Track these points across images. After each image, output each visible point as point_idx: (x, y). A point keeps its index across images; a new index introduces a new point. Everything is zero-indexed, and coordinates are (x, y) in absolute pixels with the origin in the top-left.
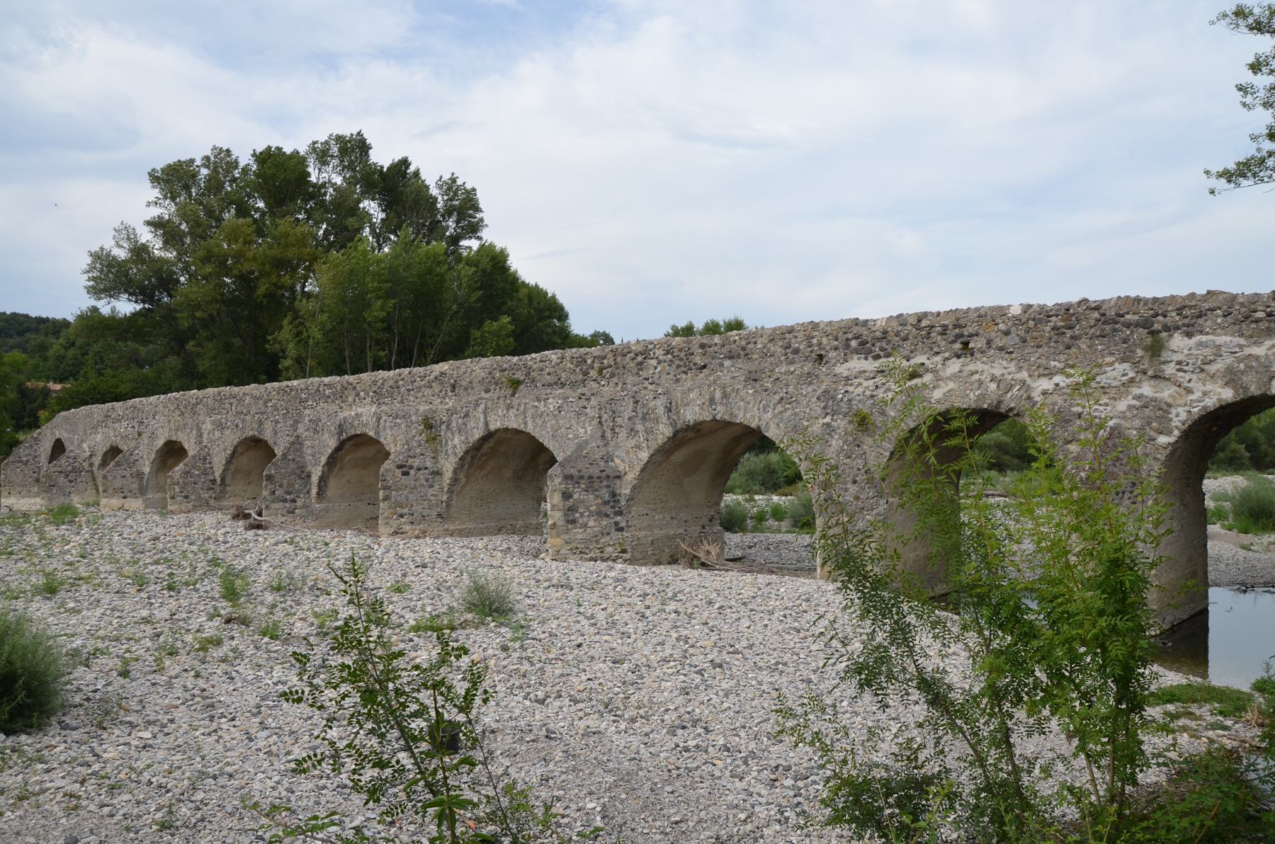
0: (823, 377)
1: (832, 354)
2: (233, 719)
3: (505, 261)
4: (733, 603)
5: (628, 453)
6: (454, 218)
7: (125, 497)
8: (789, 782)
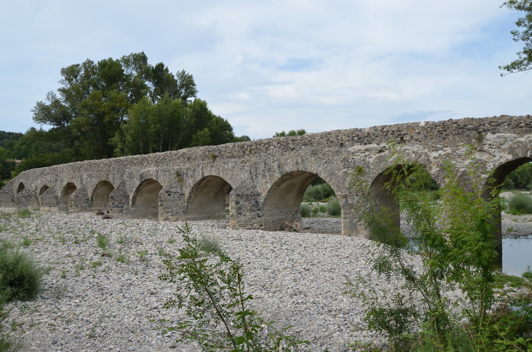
0: (343, 152)
1: (347, 143)
2: (111, 294)
3: (206, 106)
4: (310, 245)
5: (262, 185)
6: (184, 89)
7: (50, 207)
8: (341, 315)
